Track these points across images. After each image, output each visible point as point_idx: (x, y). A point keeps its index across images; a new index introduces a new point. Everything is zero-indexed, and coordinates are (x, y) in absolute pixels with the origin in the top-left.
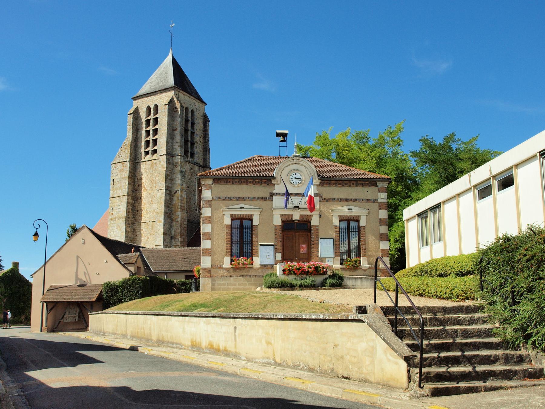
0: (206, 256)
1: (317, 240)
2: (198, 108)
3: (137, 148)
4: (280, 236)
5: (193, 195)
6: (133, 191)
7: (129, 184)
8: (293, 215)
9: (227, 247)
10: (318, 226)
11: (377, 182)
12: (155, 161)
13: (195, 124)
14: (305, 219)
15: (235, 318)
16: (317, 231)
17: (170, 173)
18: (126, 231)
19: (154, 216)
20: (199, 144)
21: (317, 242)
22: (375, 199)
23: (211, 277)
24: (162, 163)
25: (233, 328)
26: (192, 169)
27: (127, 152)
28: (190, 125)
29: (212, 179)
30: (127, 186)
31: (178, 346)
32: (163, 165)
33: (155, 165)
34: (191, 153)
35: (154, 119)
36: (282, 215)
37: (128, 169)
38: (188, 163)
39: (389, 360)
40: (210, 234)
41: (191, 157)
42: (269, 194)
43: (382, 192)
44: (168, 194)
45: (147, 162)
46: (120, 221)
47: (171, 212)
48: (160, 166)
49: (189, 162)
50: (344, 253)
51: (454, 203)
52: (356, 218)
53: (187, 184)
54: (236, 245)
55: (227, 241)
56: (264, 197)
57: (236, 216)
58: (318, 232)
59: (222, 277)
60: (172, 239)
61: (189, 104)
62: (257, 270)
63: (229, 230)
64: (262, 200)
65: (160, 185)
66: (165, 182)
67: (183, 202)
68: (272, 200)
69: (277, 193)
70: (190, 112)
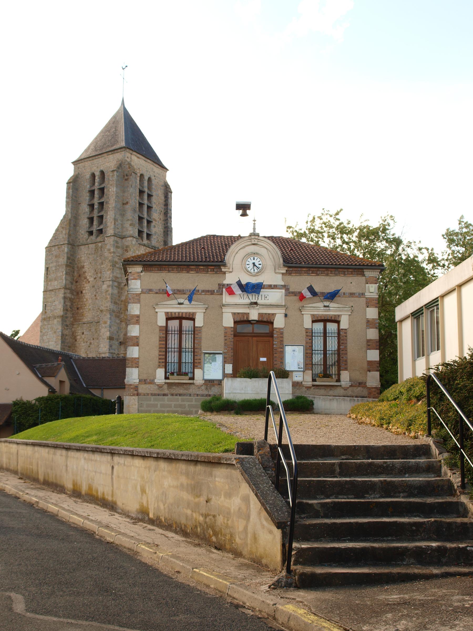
1: (281, 348)
2: (157, 175)
3: (78, 228)
4: (231, 342)
6: (72, 283)
7: (66, 274)
8: (249, 313)
10: (282, 329)
12: (100, 244)
13: (153, 196)
15: (112, 453)
16: (281, 335)
17: (118, 259)
18: (63, 335)
20: (159, 223)
21: (282, 350)
22: (361, 292)
23: (138, 395)
25: (111, 468)
27: (64, 232)
28: (146, 197)
29: (141, 266)
30: (64, 276)
36: (234, 314)
37: (66, 255)
39: (263, 526)
41: (147, 239)
42: (217, 286)
43: (370, 284)
44: (115, 286)
46: (55, 321)
47: (119, 310)
49: (144, 245)
50: (332, 365)
51: (454, 296)
52: (335, 318)
56: (210, 289)
57: (173, 314)
58: (282, 337)
59: (152, 395)
60: (120, 345)
62: (199, 387)
63: (163, 334)
64: (208, 293)
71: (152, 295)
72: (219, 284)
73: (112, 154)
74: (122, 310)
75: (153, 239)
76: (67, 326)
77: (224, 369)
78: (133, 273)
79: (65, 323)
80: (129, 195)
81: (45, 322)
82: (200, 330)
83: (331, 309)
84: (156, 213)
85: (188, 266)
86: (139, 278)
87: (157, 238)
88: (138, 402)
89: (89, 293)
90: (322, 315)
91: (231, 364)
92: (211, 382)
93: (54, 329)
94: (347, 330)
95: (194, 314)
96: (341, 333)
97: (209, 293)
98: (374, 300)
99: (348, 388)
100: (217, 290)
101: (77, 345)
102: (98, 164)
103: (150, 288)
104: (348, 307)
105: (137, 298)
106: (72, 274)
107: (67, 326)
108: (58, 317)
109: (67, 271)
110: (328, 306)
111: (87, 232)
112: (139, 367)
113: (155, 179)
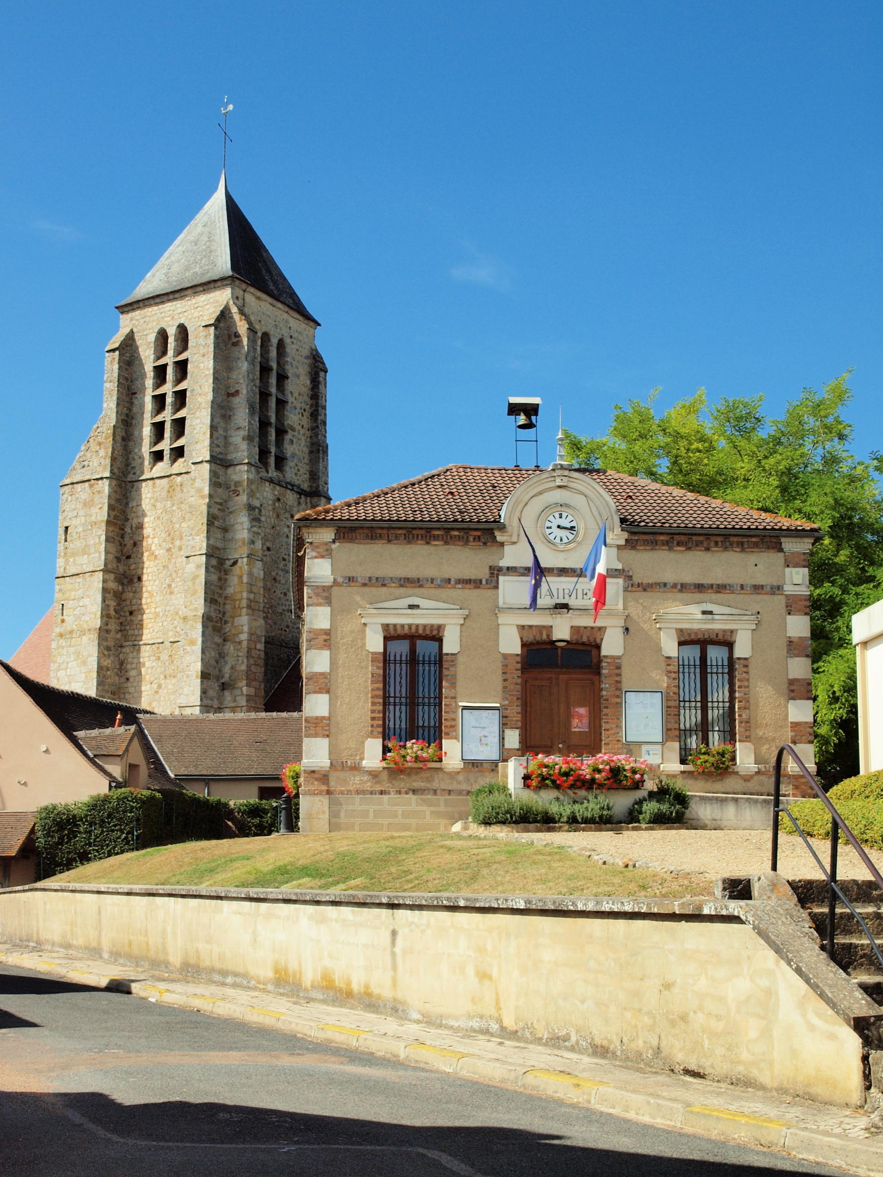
0: (316, 735)
1: (618, 697)
2: (295, 335)
3: (131, 444)
4: (516, 684)
5: (282, 570)
6: (118, 559)
7: (107, 540)
9: (373, 711)
10: (619, 657)
11: (783, 540)
12: (179, 479)
13: (288, 378)
14: (585, 639)
16: (618, 671)
17: (219, 510)
19: (176, 627)
22: (775, 584)
23: (328, 792)
24: (198, 484)
26: (279, 500)
27: (102, 453)
28: (273, 380)
29: (332, 529)
30: (104, 545)
31: (238, 980)
32: (199, 490)
33: (178, 489)
34: (277, 457)
35: (177, 363)
36: (522, 628)
37: (106, 501)
38: (267, 484)
40: (326, 678)
42: (487, 571)
45: (158, 481)
46: (85, 639)
47: (220, 616)
48: (193, 492)
49: (271, 481)
52: (724, 636)
53: (265, 539)
54: (398, 708)
55: (372, 697)
56: (473, 577)
57: (399, 628)
58: (619, 675)
59: (358, 792)
60: (223, 689)
61: (273, 323)
62: (453, 775)
64: (468, 586)
65: (192, 543)
66: (205, 534)
67: (255, 589)
68: (497, 587)
69: (508, 568)
70: (275, 345)
71: (355, 588)
72: (490, 567)
73: (204, 290)
75: (287, 469)
77: (502, 739)
78: (316, 544)
79: (105, 644)
81: (61, 641)
82: (452, 661)
83: (716, 617)
84: (295, 415)
85: (429, 530)
86: (327, 553)
87: (297, 465)
88: (329, 808)
89: (155, 581)
90: (699, 629)
91: (517, 728)
92: (477, 767)
93: (81, 657)
94: (750, 660)
95: (440, 628)
96: (737, 666)
97: (472, 586)
98: (801, 600)
99: (752, 777)
100: (487, 580)
101: (131, 690)
102: (174, 311)
103: (351, 575)
104: (750, 613)
105: (325, 594)
106: (119, 541)
108: (89, 630)
109: (109, 534)
110: (711, 613)
112: (331, 735)
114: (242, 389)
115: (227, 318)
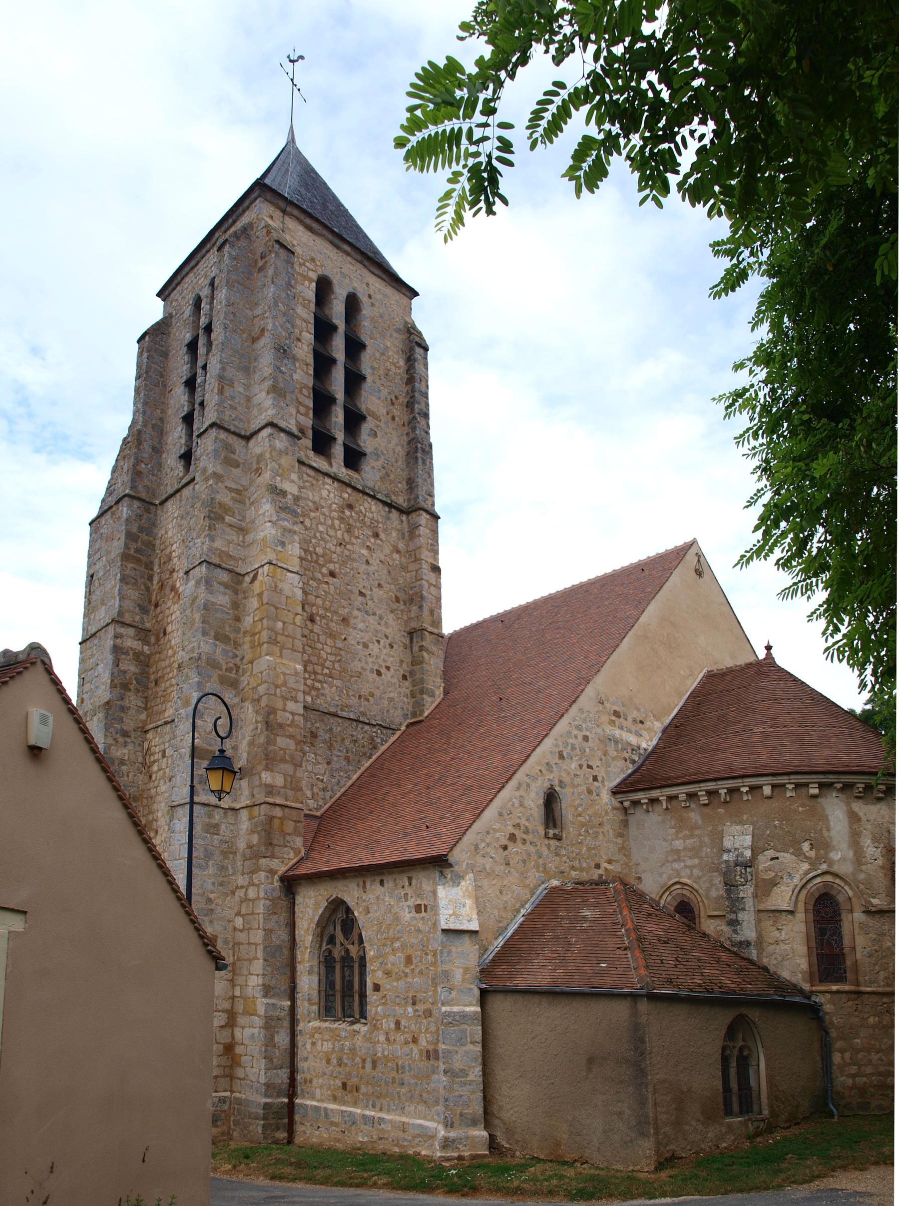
5: (359, 609)
7: (124, 580)
26: (350, 507)
34: (347, 450)
49: (335, 479)
74: (245, 661)
76: (126, 734)
80: (266, 308)
106: (145, 584)
107: (126, 734)
111: (180, 457)
113: (373, 305)
114: (268, 323)
115: (254, 239)
